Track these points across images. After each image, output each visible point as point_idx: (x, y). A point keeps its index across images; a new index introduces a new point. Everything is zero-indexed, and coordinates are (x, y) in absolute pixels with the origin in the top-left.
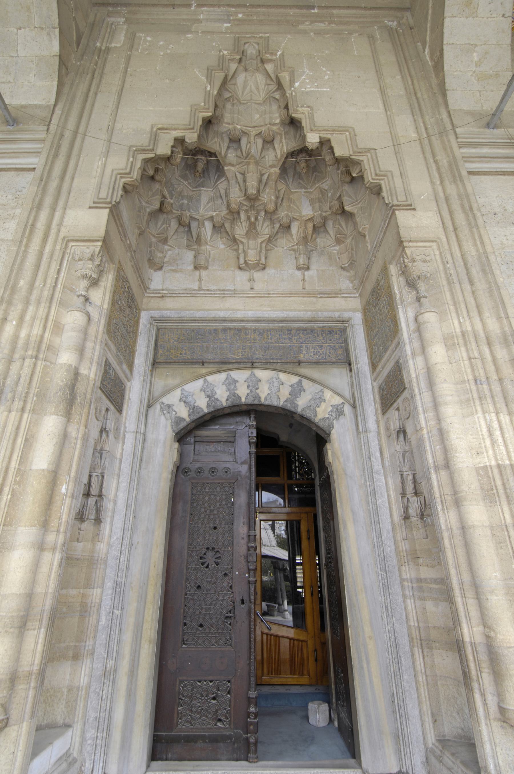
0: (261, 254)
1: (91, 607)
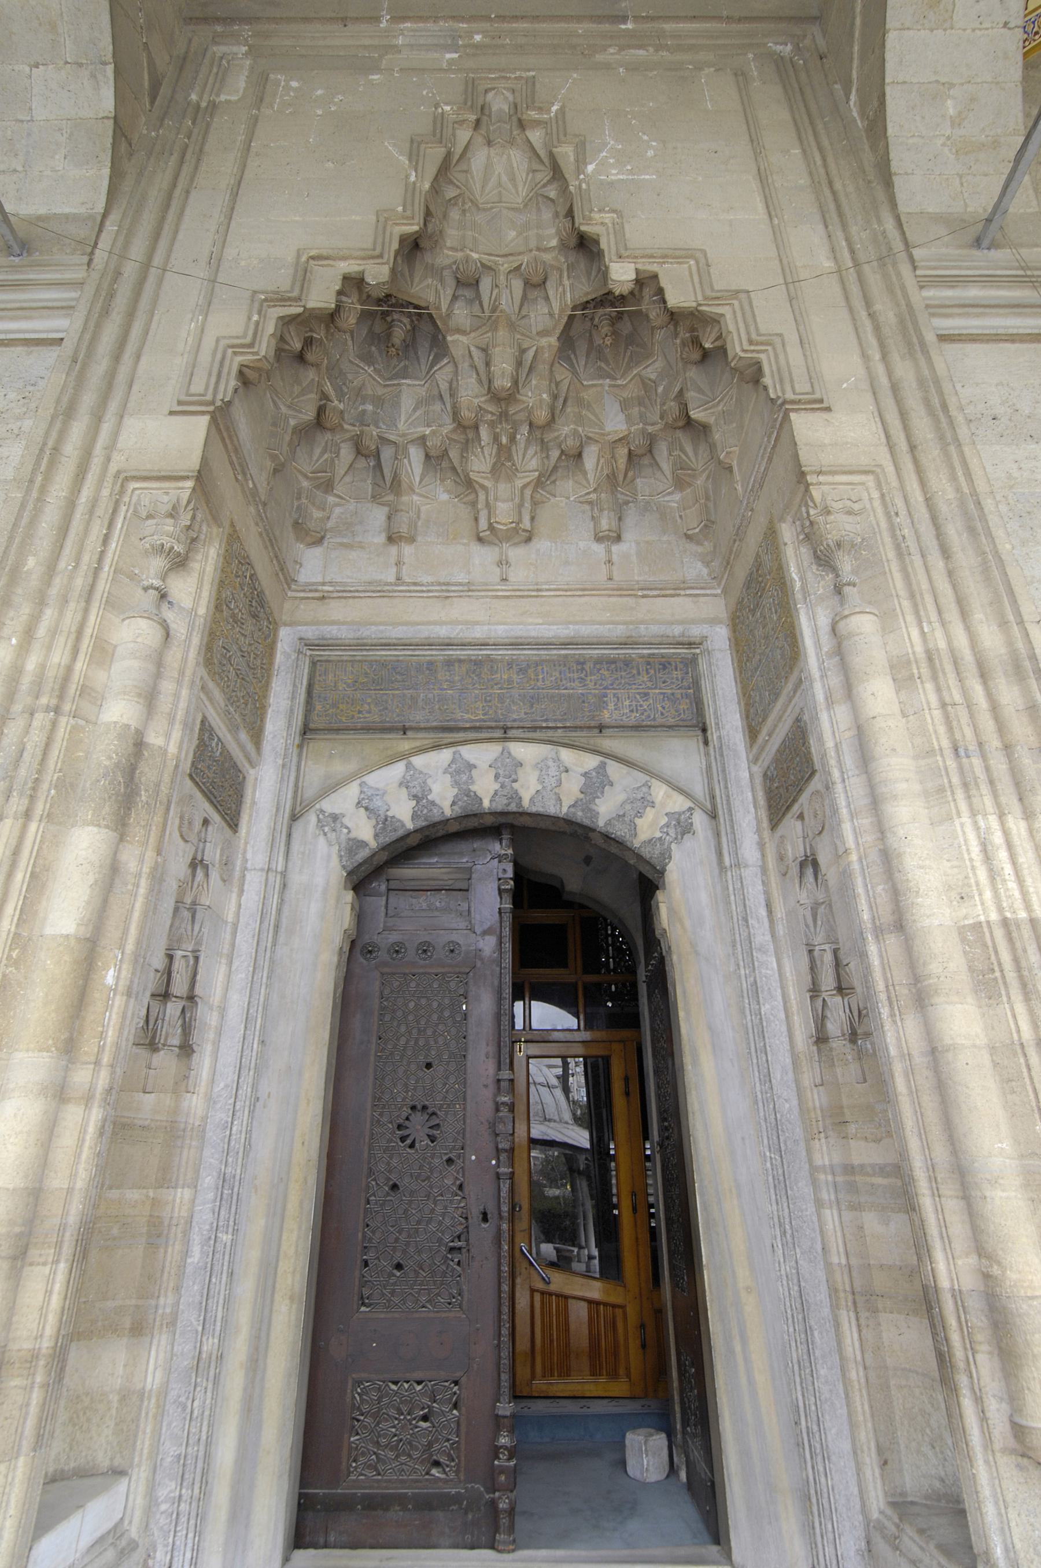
0: (523, 510)
1: (169, 1226)
